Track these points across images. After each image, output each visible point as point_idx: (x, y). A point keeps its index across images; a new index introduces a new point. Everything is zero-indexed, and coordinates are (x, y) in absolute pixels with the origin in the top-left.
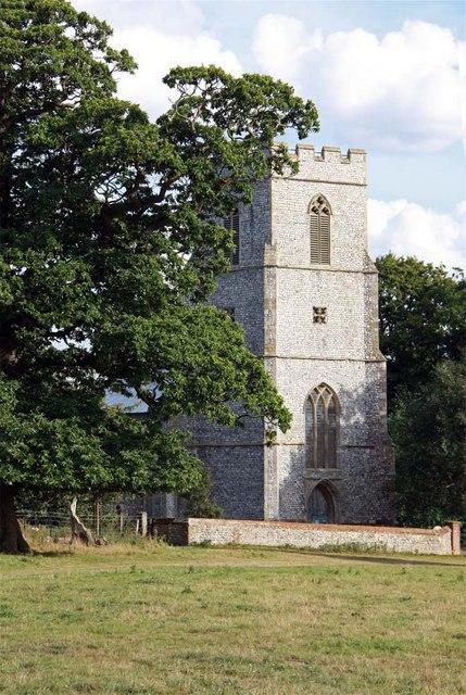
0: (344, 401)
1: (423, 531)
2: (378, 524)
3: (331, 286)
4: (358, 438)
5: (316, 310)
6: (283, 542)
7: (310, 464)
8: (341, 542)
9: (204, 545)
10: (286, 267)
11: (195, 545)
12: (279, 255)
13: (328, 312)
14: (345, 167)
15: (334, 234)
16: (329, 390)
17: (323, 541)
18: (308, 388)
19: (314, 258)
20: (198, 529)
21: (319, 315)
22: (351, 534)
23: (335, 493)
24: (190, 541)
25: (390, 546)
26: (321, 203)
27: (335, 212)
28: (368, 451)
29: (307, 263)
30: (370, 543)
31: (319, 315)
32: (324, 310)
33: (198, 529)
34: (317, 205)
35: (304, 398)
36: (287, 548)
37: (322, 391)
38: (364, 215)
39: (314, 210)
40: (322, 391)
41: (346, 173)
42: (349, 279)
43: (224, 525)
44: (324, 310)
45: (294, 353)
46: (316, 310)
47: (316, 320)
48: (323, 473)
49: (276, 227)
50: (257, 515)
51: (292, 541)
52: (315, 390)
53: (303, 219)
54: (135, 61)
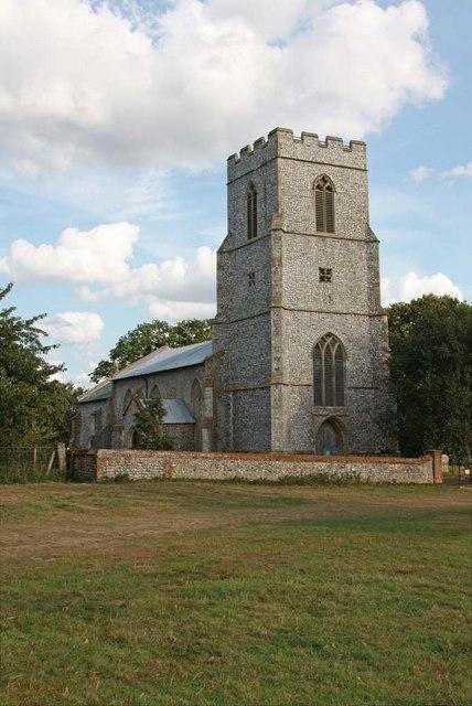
0: (350, 349)
1: (403, 460)
2: (383, 453)
3: (336, 251)
4: (363, 380)
5: (321, 270)
6: (232, 474)
7: (318, 401)
8: (307, 472)
9: (121, 479)
10: (292, 233)
11: (107, 480)
12: (286, 222)
13: (334, 274)
14: (347, 154)
15: (338, 208)
16: (336, 340)
17: (284, 472)
18: (316, 337)
19: (319, 226)
20: (111, 463)
21: (325, 275)
22: (317, 464)
23: (343, 427)
24: (99, 476)
25: (364, 476)
26: (326, 182)
27: (338, 190)
28: (373, 391)
29: (313, 230)
30: (340, 473)
31: (325, 275)
32: (329, 271)
33: (111, 463)
34: (322, 184)
35: (311, 345)
36: (236, 481)
37: (329, 340)
38: (366, 195)
39: (318, 187)
40: (329, 340)
41: (346, 158)
42: (353, 246)
43: (150, 456)
44: (329, 271)
45: (302, 306)
46: (321, 270)
47: (322, 279)
48: (330, 411)
49: (283, 199)
50: (265, 450)
51: (242, 473)
52: (323, 338)
53: (309, 194)
54: (264, 133)
